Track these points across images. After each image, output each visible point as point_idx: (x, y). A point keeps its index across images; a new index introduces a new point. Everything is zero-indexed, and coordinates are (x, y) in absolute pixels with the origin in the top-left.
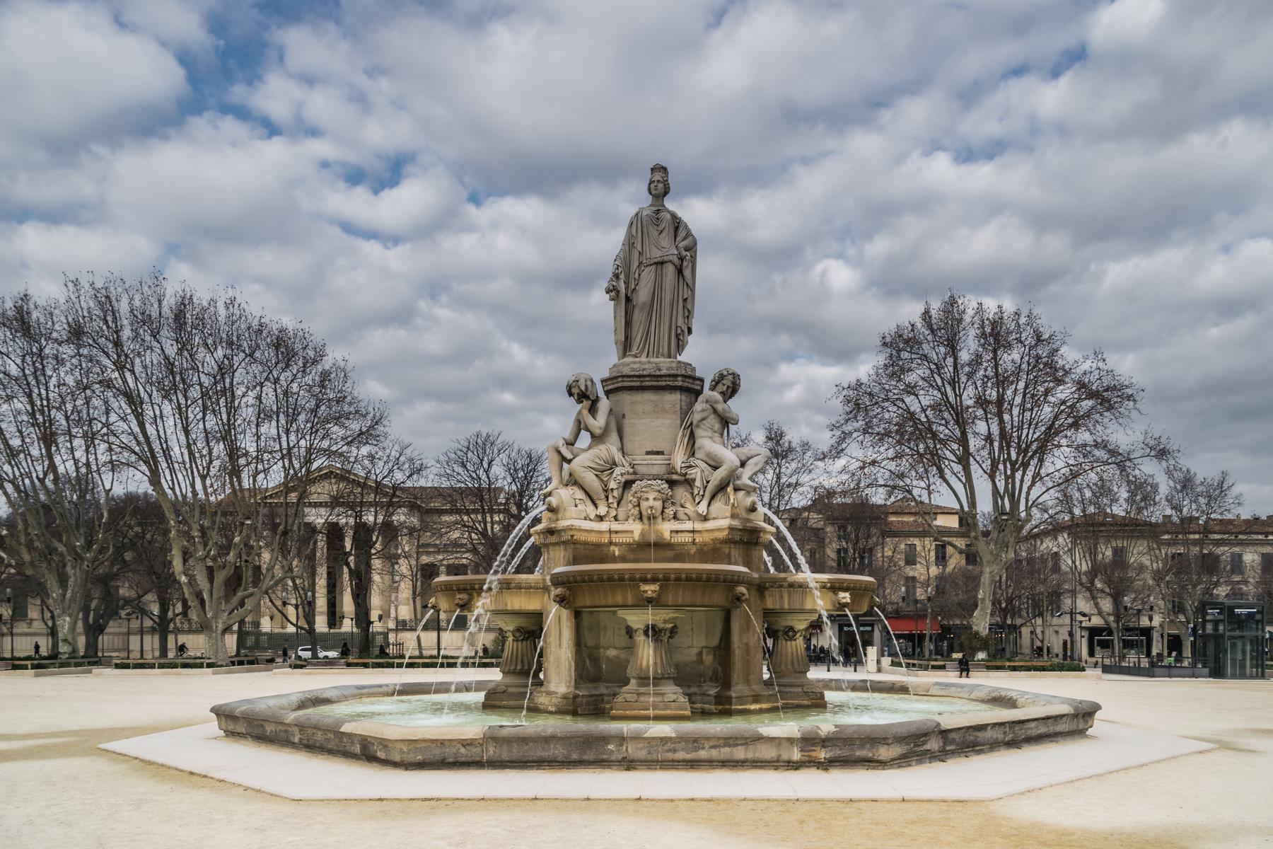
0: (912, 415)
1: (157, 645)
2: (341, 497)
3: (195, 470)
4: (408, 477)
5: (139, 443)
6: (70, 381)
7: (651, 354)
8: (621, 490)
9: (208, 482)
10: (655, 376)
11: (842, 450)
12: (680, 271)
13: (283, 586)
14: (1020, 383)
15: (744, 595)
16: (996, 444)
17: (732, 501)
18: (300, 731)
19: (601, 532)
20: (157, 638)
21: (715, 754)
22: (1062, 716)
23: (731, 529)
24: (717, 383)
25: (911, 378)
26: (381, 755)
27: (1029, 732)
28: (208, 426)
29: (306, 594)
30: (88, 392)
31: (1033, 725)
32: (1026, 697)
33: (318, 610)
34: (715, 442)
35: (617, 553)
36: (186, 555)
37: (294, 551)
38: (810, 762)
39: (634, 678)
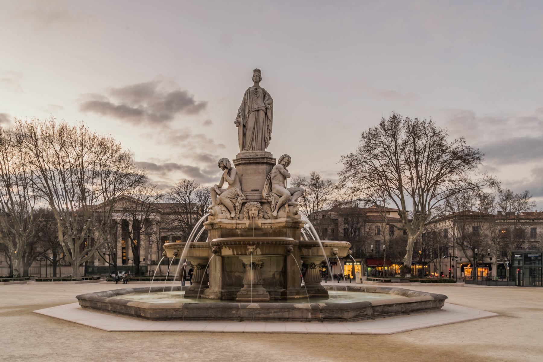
0: (376, 169)
1: (52, 272)
2: (127, 209)
3: (67, 198)
4: (155, 200)
5: (45, 187)
6: (17, 162)
7: (253, 149)
8: (241, 206)
9: (73, 203)
10: (255, 158)
11: (344, 185)
12: (266, 114)
13: (104, 246)
14: (425, 153)
15: (291, 250)
16: (415, 181)
17: (287, 210)
18: (111, 305)
19: (233, 224)
20: (52, 269)
21: (276, 315)
22: (429, 301)
23: (287, 222)
24: (281, 161)
25: (376, 152)
26: (143, 315)
27: (413, 308)
28: (73, 180)
29: (113, 250)
30: (25, 166)
31: (415, 304)
32: (416, 293)
33: (118, 256)
34: (280, 186)
35: (239, 233)
36: (64, 234)
37: (108, 232)
38: (315, 319)
39: (246, 284)
